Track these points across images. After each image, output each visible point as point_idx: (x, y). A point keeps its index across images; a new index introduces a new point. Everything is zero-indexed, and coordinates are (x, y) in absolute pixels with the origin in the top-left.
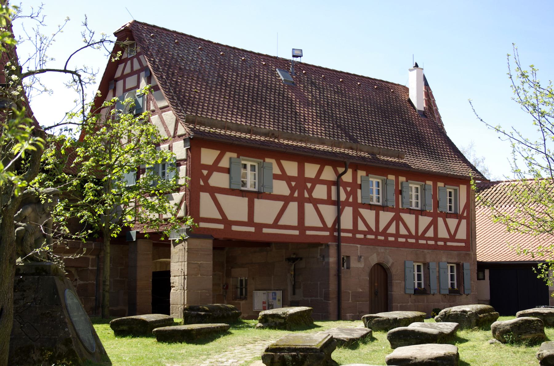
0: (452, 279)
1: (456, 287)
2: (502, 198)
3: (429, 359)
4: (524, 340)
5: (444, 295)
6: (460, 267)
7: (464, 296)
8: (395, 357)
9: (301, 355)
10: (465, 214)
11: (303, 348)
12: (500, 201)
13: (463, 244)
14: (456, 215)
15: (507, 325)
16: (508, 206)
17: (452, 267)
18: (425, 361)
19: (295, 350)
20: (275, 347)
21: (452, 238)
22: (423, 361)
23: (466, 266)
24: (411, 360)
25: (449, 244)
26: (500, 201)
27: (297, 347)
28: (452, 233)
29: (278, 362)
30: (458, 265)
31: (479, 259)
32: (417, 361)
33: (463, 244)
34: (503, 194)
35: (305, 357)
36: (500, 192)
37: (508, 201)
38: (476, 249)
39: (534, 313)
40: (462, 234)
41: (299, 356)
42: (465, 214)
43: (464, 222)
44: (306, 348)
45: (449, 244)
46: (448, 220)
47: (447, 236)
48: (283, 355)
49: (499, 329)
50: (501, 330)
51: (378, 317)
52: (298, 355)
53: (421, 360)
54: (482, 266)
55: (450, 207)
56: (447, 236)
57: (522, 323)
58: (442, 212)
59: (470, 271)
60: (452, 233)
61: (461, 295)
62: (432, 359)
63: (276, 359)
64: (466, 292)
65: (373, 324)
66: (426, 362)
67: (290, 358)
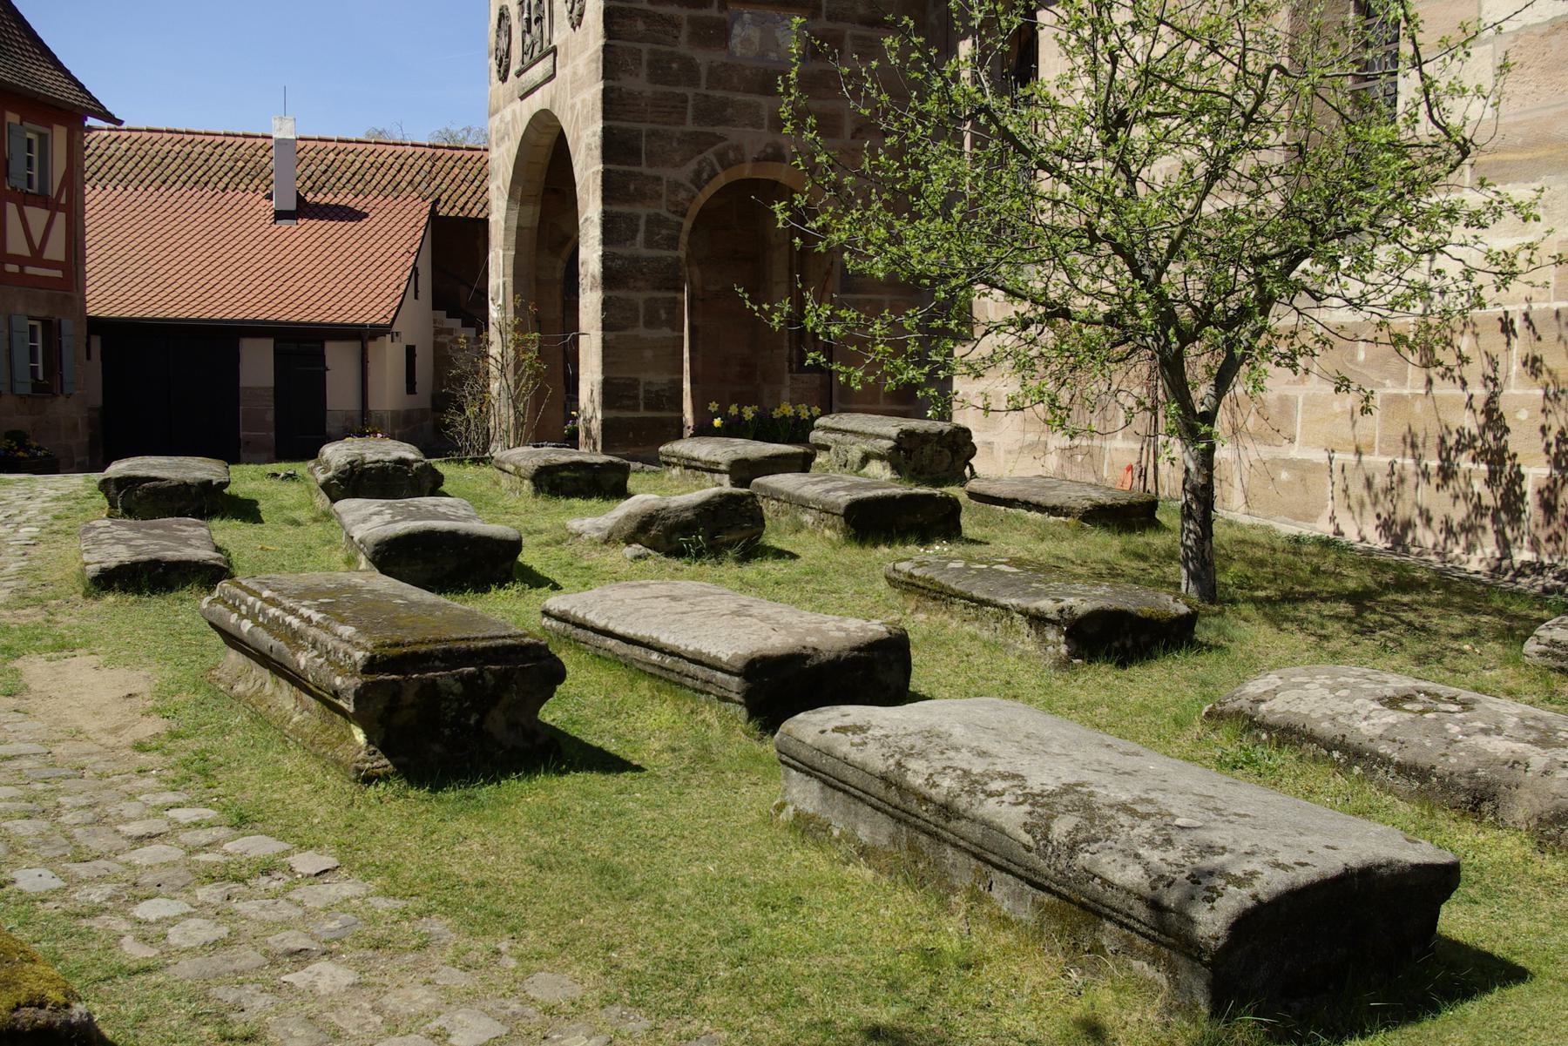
0: (33, 358)
1: (41, 377)
2: (105, 169)
3: (853, 649)
4: (730, 545)
5: (21, 396)
6: (51, 328)
7: (61, 399)
8: (766, 653)
9: (493, 673)
10: (63, 201)
11: (496, 649)
12: (99, 175)
13: (58, 274)
14: (42, 200)
15: (687, 509)
16: (120, 188)
17: (32, 328)
18: (844, 654)
19: (470, 656)
20: (396, 651)
21: (37, 257)
22: (839, 657)
23: (67, 326)
24: (808, 657)
25: (30, 270)
26: (99, 175)
27: (472, 645)
28: (37, 242)
29: (412, 705)
30: (47, 323)
31: (93, 310)
32: (823, 658)
33: (58, 274)
34: (105, 158)
35: (504, 678)
36: (98, 152)
37: (120, 176)
38: (85, 287)
39: (573, 463)
40: (56, 250)
41: (488, 677)
42: (63, 201)
43: (61, 217)
44: (504, 647)
45: (30, 270)
46: (29, 210)
47: (26, 252)
48: (433, 681)
49: (663, 518)
50: (669, 522)
51: (155, 479)
52: (481, 675)
53: (832, 656)
54: (99, 326)
55: (30, 177)
56: (26, 252)
57: (721, 504)
58: (14, 189)
59: (72, 334)
60: (37, 242)
61: (55, 395)
62: (859, 649)
63: (409, 696)
64: (66, 391)
65: (140, 499)
66: (846, 659)
67: (457, 688)
